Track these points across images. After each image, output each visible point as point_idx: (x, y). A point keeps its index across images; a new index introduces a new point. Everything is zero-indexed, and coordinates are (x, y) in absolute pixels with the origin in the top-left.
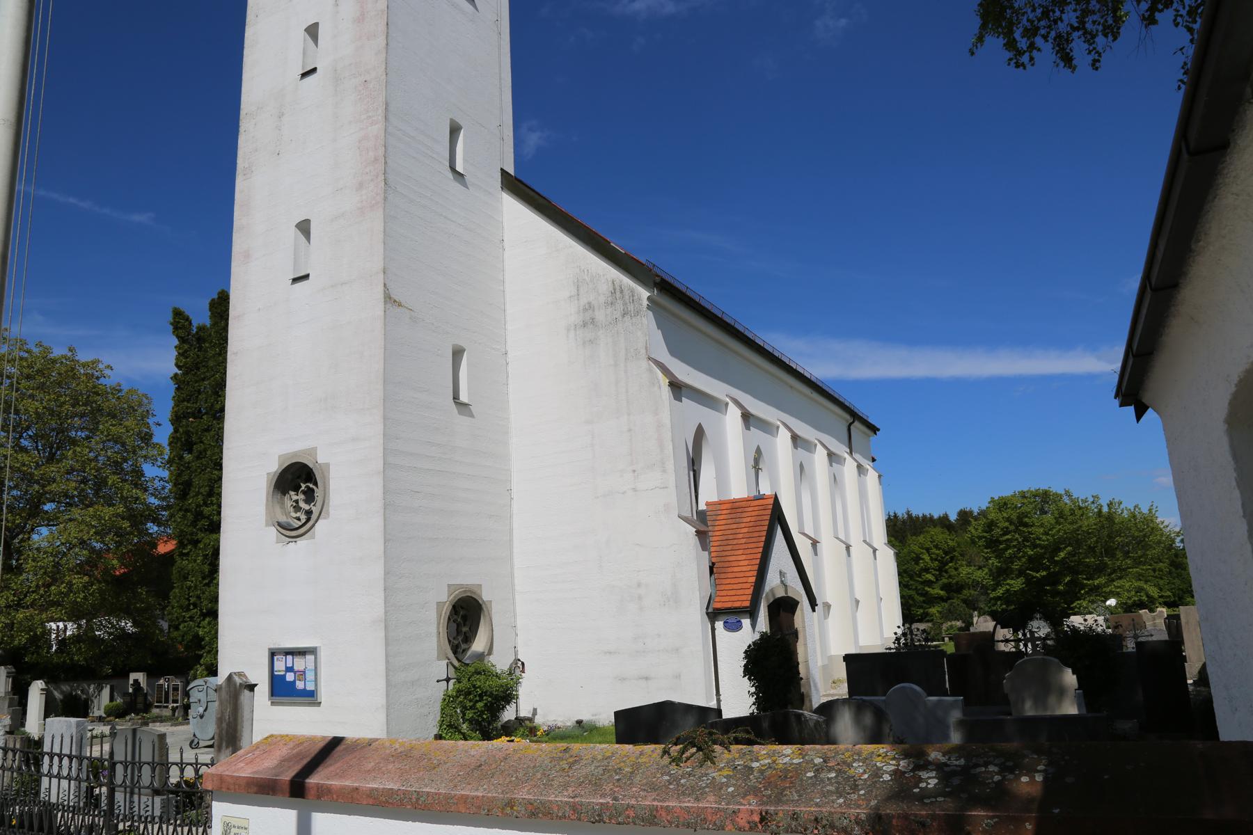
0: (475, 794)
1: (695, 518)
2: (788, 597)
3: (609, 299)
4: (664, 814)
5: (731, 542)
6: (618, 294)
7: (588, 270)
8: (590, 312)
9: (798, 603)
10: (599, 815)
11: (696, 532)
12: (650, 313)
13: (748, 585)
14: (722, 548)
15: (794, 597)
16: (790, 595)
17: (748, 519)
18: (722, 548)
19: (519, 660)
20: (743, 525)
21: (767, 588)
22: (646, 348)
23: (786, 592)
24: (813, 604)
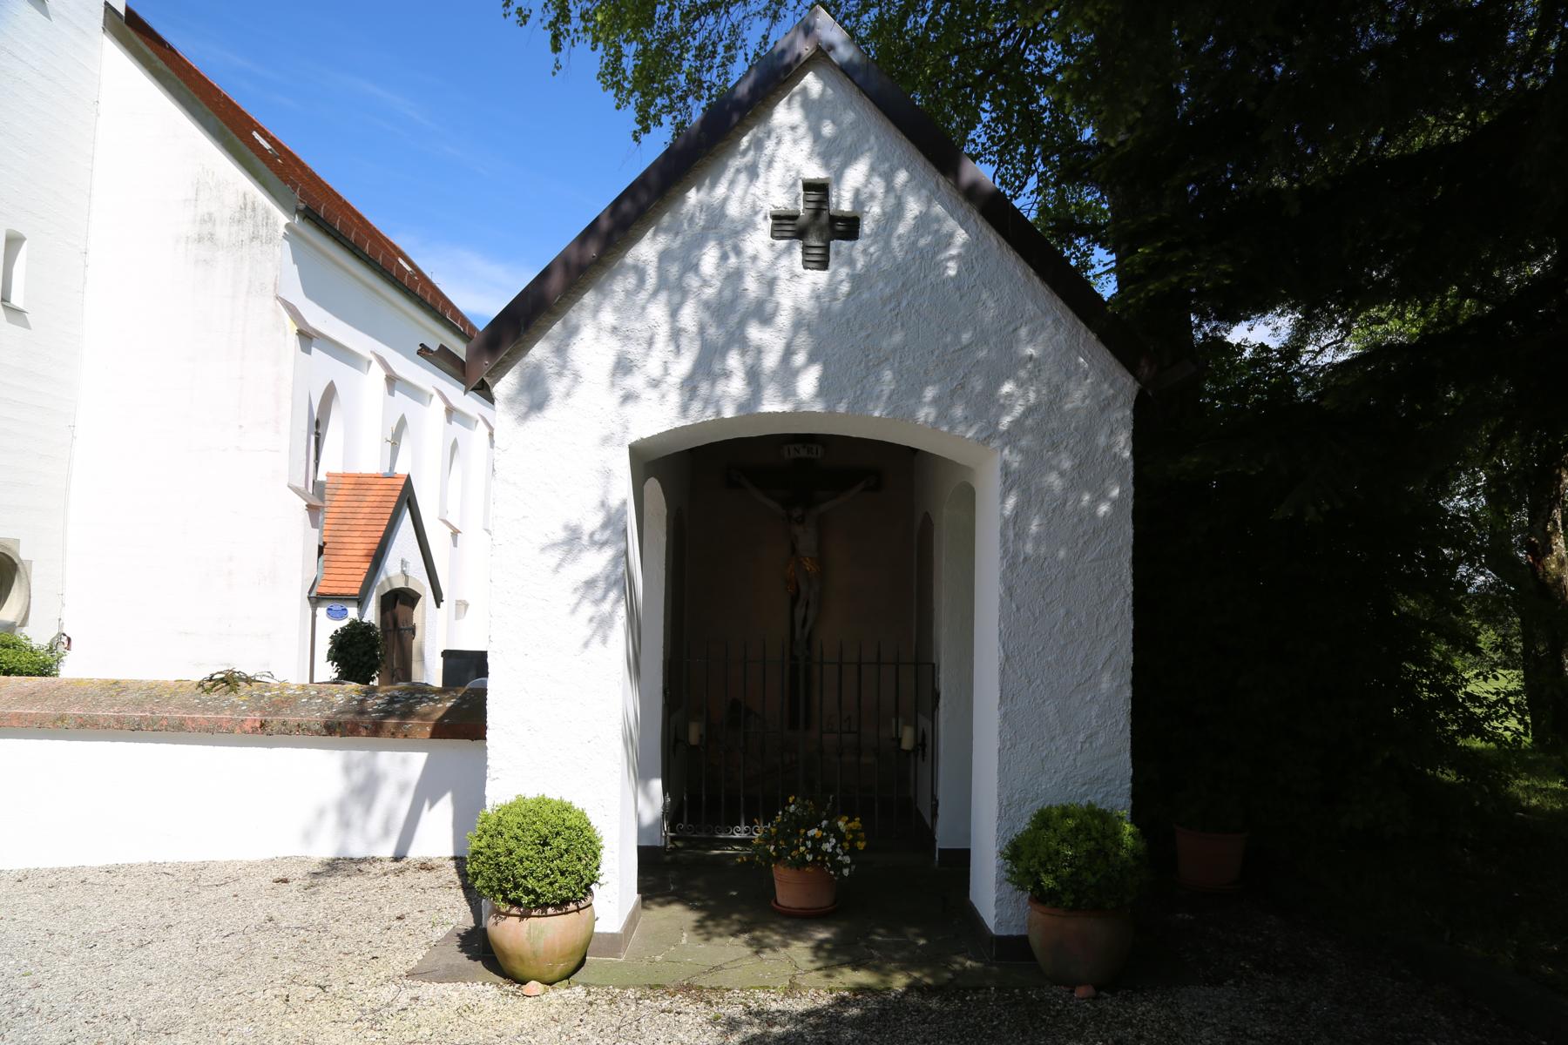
0: (30, 711)
1: (310, 490)
2: (408, 589)
3: (237, 215)
4: (190, 723)
5: (348, 522)
6: (249, 212)
7: (213, 173)
9: (420, 596)
10: (138, 725)
11: (307, 506)
12: (287, 243)
13: (361, 571)
14: (336, 527)
15: (416, 590)
16: (410, 586)
17: (373, 499)
18: (336, 527)
19: (64, 635)
20: (366, 504)
21: (382, 577)
22: (275, 284)
23: (407, 583)
24: (438, 598)
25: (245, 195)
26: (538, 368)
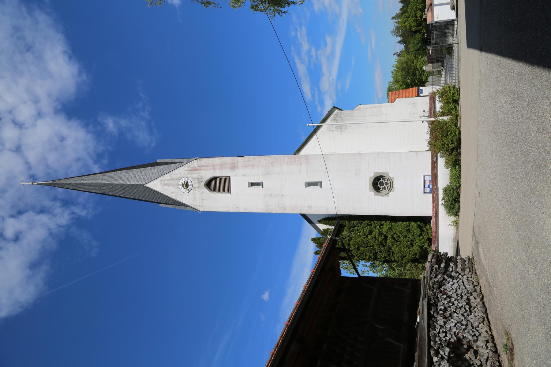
6: (335, 119)
8: (338, 127)
17: (395, 97)
25: (331, 120)
26: (432, 38)
